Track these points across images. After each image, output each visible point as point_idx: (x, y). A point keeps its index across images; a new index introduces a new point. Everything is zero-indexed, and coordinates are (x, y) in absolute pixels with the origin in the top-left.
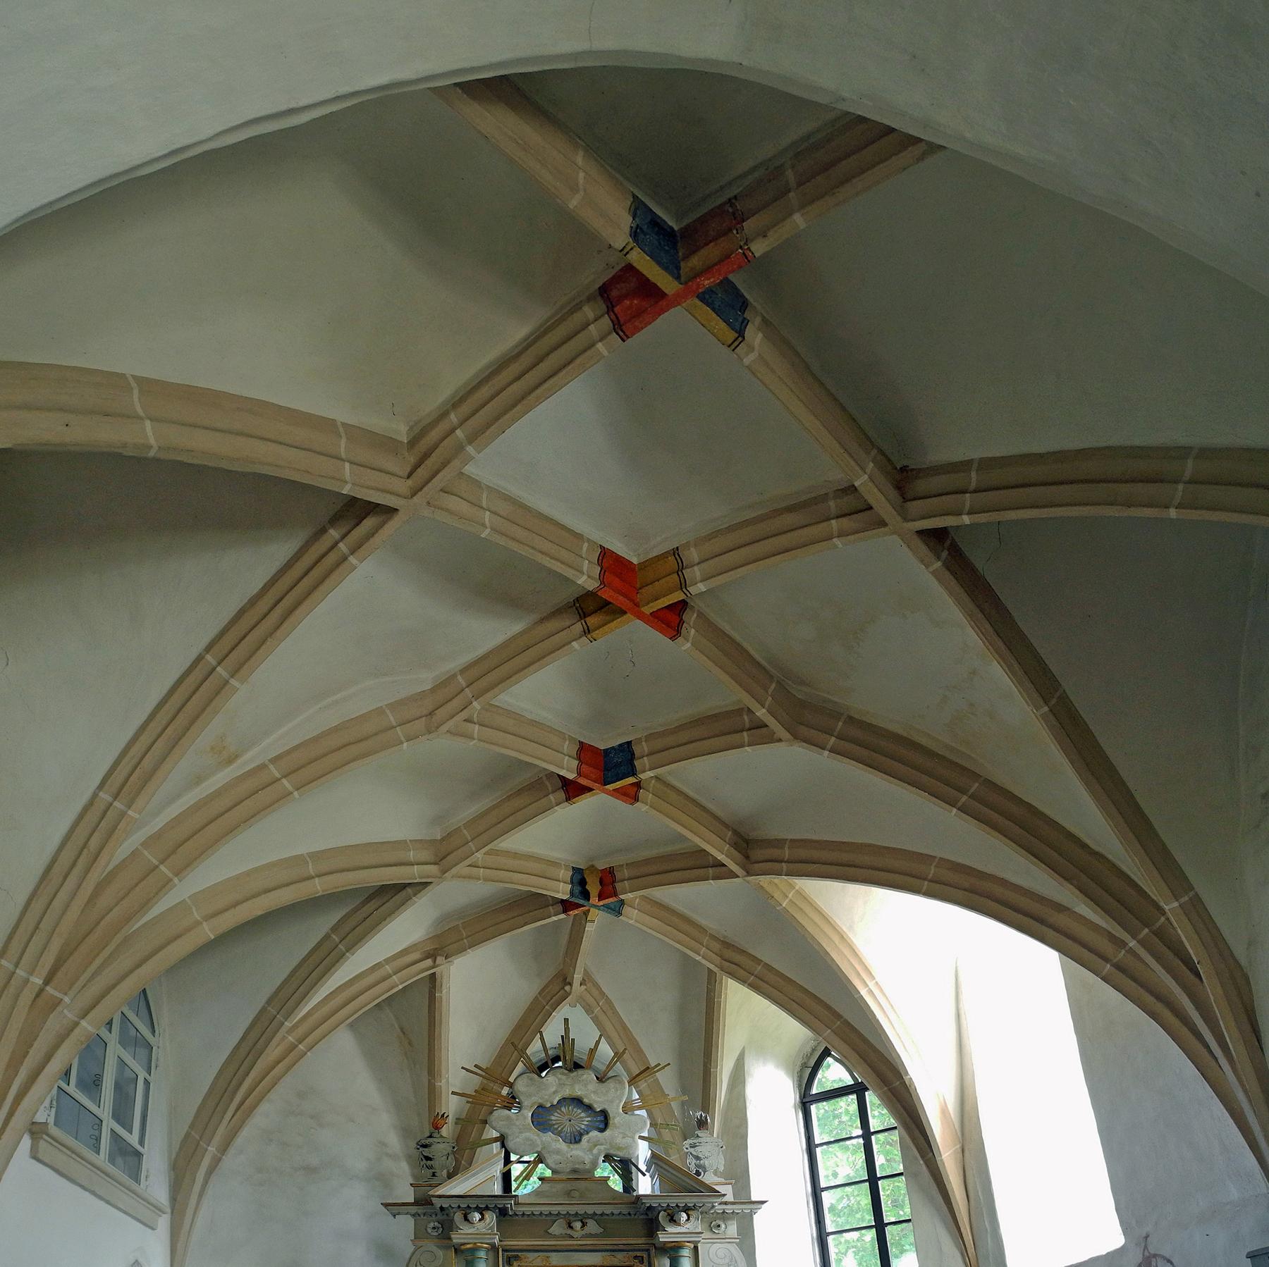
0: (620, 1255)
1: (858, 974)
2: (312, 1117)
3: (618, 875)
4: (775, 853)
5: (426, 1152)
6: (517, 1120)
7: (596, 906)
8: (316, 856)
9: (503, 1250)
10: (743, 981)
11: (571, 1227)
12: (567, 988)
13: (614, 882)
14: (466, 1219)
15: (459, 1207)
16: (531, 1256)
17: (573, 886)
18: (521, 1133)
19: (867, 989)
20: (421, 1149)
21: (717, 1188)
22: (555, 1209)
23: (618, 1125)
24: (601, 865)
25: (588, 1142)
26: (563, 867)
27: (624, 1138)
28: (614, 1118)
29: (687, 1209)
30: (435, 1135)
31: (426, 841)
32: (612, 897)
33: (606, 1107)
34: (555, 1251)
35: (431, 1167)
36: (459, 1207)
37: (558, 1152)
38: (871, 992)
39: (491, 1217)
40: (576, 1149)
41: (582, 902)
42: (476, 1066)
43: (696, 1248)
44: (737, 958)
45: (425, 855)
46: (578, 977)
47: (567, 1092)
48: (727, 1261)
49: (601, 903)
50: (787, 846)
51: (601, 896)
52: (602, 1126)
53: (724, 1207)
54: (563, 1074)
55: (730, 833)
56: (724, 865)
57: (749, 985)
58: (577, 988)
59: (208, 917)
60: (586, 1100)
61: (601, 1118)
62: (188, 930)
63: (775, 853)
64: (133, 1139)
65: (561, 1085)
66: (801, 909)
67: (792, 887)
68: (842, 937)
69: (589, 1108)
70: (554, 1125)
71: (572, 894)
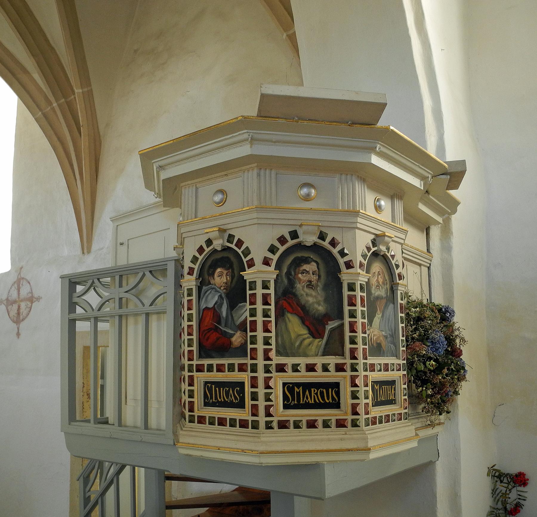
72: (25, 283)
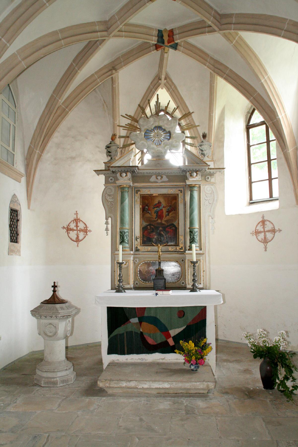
0: (174, 190)
1: (261, 73)
2: (73, 137)
3: (175, 33)
4: (228, 20)
5: (109, 150)
6: (139, 136)
7: (167, 46)
8: (62, 31)
9: (135, 188)
10: (222, 77)
11: (157, 179)
12: (160, 81)
13: (173, 35)
14: (121, 176)
15: (118, 171)
16: (144, 190)
17: (158, 38)
18: (140, 141)
19: (264, 79)
20: (107, 148)
21: (207, 163)
22: (151, 171)
23: (174, 137)
24: (168, 28)
25: (164, 144)
26: (155, 30)
27: (176, 142)
28: (173, 134)
29: (196, 171)
30: (112, 143)
31: (100, 22)
32: (172, 42)
33: (170, 130)
34: (153, 188)
35: (110, 156)
36: (118, 171)
37: (153, 149)
38: (266, 81)
39: (129, 174)
40: (159, 147)
41: (161, 45)
42: (126, 115)
43: (200, 187)
44: (221, 67)
45: (102, 28)
46: (163, 77)
47: (157, 124)
48: (210, 192)
49: (169, 45)
50: (234, 16)
51: (168, 43)
52: (169, 138)
53: (210, 170)
54: (155, 117)
55: (213, 11)
56: (211, 26)
57: (224, 78)
58: (163, 81)
59: (24, 59)
60: (163, 127)
61: (168, 134)
62: (17, 65)
63: (228, 20)
64: (10, 149)
65: (155, 121)
66: (240, 45)
67: (237, 34)
68: (256, 56)
69: (164, 130)
70: (152, 137)
71: (158, 41)
72: (75, 239)
